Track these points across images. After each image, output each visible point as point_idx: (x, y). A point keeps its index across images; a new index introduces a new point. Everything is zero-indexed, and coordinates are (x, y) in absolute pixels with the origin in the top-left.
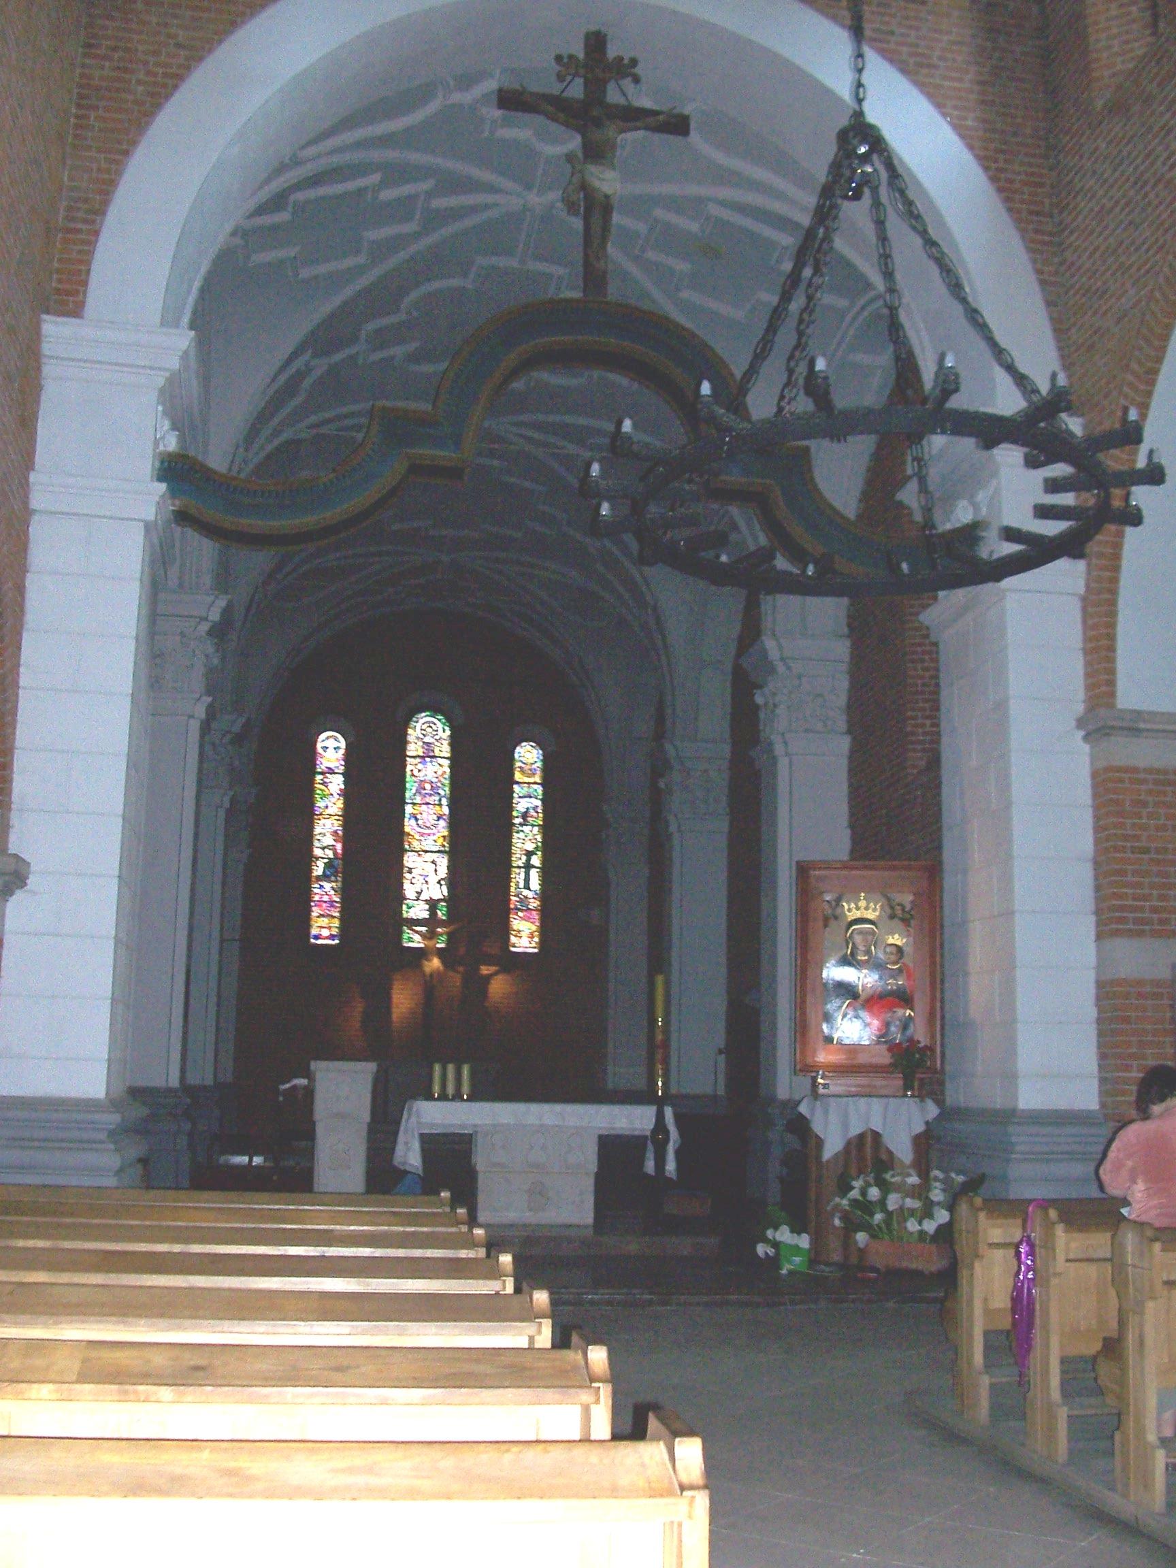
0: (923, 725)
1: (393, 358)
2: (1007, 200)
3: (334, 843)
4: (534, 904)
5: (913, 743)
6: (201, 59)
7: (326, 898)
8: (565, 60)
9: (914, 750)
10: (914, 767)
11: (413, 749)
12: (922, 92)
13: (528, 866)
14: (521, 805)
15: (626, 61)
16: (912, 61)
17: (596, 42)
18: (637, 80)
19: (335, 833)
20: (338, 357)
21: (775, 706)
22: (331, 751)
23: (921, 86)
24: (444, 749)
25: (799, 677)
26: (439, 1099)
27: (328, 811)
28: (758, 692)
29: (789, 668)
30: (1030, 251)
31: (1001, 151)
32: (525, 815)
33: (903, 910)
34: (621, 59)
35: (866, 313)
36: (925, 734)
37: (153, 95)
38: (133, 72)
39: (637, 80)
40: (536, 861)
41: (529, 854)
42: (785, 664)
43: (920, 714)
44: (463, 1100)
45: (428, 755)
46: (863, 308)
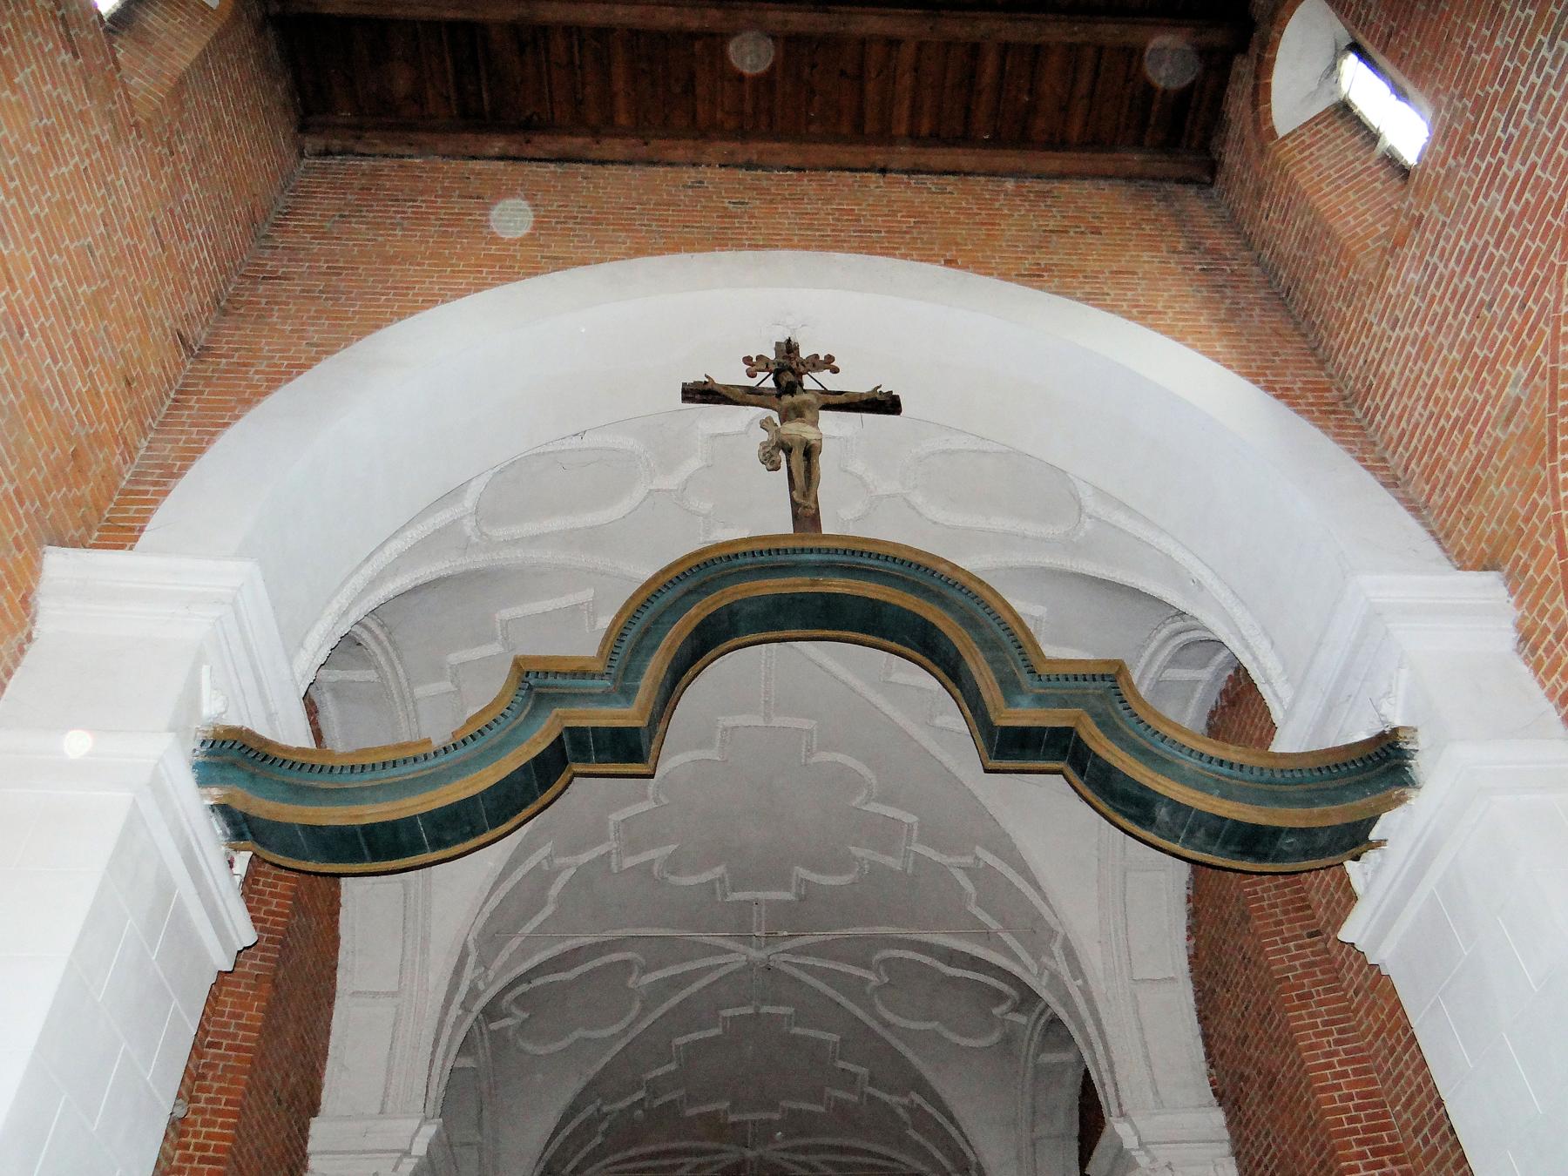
2: (1291, 404)
15: (822, 358)
17: (789, 349)
18: (835, 371)
20: (584, 858)
25: (1169, 1166)
29: (1154, 1160)
34: (817, 356)
37: (267, 380)
38: (252, 365)
39: (835, 371)
42: (1147, 1152)
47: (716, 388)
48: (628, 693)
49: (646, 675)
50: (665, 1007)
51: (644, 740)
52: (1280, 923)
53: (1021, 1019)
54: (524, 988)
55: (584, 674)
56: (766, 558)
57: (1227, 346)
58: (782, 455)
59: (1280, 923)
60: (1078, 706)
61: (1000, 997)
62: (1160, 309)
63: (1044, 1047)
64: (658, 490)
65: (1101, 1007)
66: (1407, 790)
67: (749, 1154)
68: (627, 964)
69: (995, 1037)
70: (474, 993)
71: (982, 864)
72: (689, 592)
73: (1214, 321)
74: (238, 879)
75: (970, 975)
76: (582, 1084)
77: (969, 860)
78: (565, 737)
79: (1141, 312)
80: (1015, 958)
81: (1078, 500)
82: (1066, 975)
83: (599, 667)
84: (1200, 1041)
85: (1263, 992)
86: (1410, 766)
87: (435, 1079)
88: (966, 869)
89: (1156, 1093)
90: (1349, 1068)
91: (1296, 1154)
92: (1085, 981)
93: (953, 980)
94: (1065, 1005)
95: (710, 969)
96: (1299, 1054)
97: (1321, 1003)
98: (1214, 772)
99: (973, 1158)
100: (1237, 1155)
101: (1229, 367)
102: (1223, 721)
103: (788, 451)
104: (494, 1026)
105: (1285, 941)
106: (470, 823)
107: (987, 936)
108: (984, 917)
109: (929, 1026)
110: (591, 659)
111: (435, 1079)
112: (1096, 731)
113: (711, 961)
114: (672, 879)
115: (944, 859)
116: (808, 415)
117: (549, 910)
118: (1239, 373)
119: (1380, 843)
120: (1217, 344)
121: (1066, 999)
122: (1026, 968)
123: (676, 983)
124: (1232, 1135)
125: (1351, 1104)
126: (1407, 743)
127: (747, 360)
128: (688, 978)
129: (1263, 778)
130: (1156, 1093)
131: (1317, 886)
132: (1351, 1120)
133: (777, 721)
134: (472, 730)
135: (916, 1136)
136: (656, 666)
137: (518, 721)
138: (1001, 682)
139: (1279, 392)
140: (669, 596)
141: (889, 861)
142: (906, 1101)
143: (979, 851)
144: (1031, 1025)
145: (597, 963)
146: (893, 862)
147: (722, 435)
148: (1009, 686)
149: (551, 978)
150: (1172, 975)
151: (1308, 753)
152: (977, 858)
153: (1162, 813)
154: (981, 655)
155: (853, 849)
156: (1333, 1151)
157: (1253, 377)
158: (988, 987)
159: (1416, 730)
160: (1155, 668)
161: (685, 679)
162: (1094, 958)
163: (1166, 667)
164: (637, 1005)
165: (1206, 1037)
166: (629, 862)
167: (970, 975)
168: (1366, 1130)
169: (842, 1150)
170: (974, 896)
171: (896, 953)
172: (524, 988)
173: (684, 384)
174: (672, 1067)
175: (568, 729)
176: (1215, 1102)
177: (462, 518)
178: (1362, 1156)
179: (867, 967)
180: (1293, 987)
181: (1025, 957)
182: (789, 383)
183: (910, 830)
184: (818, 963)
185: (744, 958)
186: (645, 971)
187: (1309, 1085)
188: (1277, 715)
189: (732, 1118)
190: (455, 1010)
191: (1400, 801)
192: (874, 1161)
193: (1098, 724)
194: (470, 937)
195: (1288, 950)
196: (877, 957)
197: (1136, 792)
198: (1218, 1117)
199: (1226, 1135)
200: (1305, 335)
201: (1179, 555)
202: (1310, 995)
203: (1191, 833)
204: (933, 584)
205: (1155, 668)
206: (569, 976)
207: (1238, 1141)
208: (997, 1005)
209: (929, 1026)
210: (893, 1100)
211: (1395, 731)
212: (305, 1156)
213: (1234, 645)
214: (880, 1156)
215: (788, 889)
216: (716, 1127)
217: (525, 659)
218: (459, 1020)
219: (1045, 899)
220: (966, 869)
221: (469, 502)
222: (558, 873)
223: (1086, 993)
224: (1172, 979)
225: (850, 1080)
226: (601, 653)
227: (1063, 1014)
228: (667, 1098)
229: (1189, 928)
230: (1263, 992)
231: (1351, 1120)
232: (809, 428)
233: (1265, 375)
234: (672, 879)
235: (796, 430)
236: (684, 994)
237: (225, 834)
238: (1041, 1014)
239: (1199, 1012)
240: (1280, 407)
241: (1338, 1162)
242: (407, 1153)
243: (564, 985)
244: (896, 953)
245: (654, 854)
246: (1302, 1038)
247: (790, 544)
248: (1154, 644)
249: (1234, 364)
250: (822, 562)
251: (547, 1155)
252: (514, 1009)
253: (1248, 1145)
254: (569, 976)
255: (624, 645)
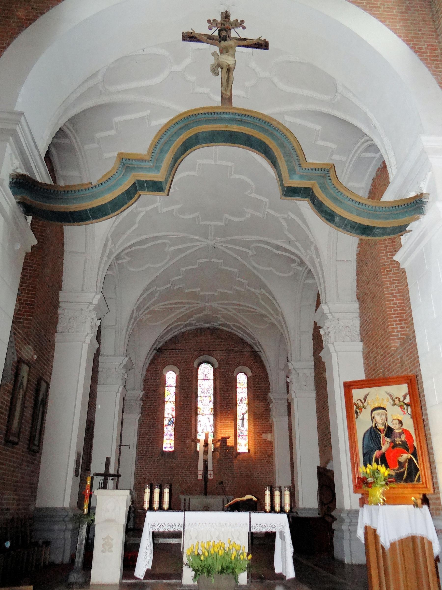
0: (397, 328)
1: (173, 210)
2: (419, 56)
3: (172, 412)
4: (246, 433)
5: (392, 336)
6: (42, 14)
7: (169, 433)
8: (212, 22)
9: (394, 339)
10: (394, 346)
11: (200, 377)
12: (375, 17)
13: (243, 419)
14: (239, 396)
15: (239, 22)
16: (368, 6)
17: (226, 16)
18: (244, 28)
19: (173, 408)
20: (149, 208)
21: (329, 332)
22: (171, 379)
23: (374, 15)
24: (211, 377)
25: (338, 319)
26: (158, 510)
27: (170, 400)
28: (321, 330)
29: (333, 317)
30: (434, 75)
31: (415, 37)
32: (241, 400)
33: (399, 400)
34: (237, 20)
35: (355, 157)
36: (398, 332)
37: (19, 26)
38: (11, 18)
39: (244, 28)
40: (246, 416)
41: (243, 414)
42: (332, 315)
43: (394, 323)
44: (266, 512)
45: (206, 379)
46: (353, 156)
47: (195, 36)
48: (158, 168)
49: (164, 161)
50: (178, 258)
51: (164, 185)
52: (386, 246)
53: (300, 269)
54: (129, 250)
55: (142, 160)
56: (209, 116)
57: (401, 26)
58: (220, 69)
59: (386, 246)
60: (314, 180)
61: (293, 261)
62: (379, 5)
63: (307, 278)
64: (174, 72)
65: (324, 268)
66: (420, 215)
67: (207, 304)
68: (165, 244)
69: (291, 273)
70: (111, 253)
71: (290, 218)
72: (181, 129)
73: (400, 13)
74: (29, 224)
75: (284, 253)
76: (150, 281)
77: (286, 216)
78: (136, 182)
79: (371, 7)
80: (299, 250)
81: (336, 87)
82: (315, 257)
83: (148, 158)
84: (356, 281)
85: (376, 268)
86: (424, 207)
87: (99, 281)
88: (284, 219)
89: (338, 297)
90: (398, 295)
91: (377, 319)
92: (320, 260)
93: (278, 255)
94: (313, 266)
95: (193, 247)
96: (383, 289)
97: (393, 274)
98: (357, 206)
99: (280, 311)
100: (360, 317)
101: (400, 36)
102: (381, 174)
103: (222, 68)
104: (119, 262)
105: (387, 252)
106: (105, 212)
107: (290, 242)
108: (290, 235)
109: (268, 269)
110: (145, 155)
111: (99, 281)
112: (319, 190)
113: (193, 244)
114: (181, 216)
115: (278, 215)
116: (230, 51)
117: (136, 226)
118: (403, 40)
119: (410, 231)
120: (397, 25)
121: (314, 266)
122: (302, 253)
123: (181, 251)
124: (360, 311)
125: (396, 305)
126: (425, 199)
127: (209, 21)
128: (187, 249)
129: (372, 210)
130: (338, 297)
131: (393, 241)
132: (395, 310)
133: (219, 162)
134: (104, 180)
135: (263, 303)
136: (168, 157)
137: (120, 177)
138: (289, 170)
139: (417, 50)
140: (174, 130)
141: (258, 214)
142: (259, 292)
143: (290, 213)
144: (304, 270)
145: (154, 243)
146: (260, 215)
147: (199, 49)
148: (292, 171)
149: (138, 247)
150: (350, 259)
151: (389, 201)
152: (289, 216)
153: (337, 219)
154: (283, 158)
155: (245, 209)
156: (387, 319)
157: (408, 41)
158: (289, 257)
159: (429, 195)
160: (359, 152)
161: (179, 161)
162: (324, 252)
163: (363, 152)
164: (168, 257)
165: (358, 281)
166: (165, 210)
167: (284, 253)
168: (399, 314)
169: (239, 305)
170: (287, 228)
171: (259, 245)
172: (129, 250)
173: (183, 33)
174: (180, 277)
175: (137, 180)
176: (357, 300)
177: (98, 83)
178: (396, 321)
179: (249, 248)
180: (386, 268)
181: (302, 249)
182: (224, 36)
183: (266, 205)
184: (232, 246)
185: (206, 243)
186: (171, 246)
187: (385, 298)
188: (391, 178)
189: (201, 293)
190: (105, 259)
191: (417, 219)
192: (248, 309)
193: (320, 187)
194: (109, 235)
195: (387, 255)
196: (252, 246)
197: (329, 212)
198: (357, 305)
199: (358, 311)
200: (434, 21)
201: (370, 115)
202: (391, 271)
203: (346, 226)
204: (271, 130)
205: (359, 152)
206: (145, 247)
207: (361, 313)
208: (293, 263)
209: (268, 269)
210: (257, 291)
211: (422, 194)
212: (58, 302)
213: (382, 151)
214: (251, 308)
215: (222, 222)
216: (195, 296)
217: (122, 154)
218: (107, 262)
219: (310, 231)
220: (284, 219)
221: (100, 77)
222: (139, 213)
223: (320, 263)
224: (350, 261)
225: (241, 284)
226: (148, 153)
227: (312, 270)
228: (179, 286)
229: (359, 244)
230: (376, 268)
231: (395, 310)
232: (230, 58)
233: (413, 41)
234: (181, 216)
235: (227, 59)
236: (184, 254)
237: (23, 210)
238: (306, 269)
239: (357, 272)
240: (415, 57)
241: (388, 322)
242: (91, 303)
243: (145, 249)
244: (259, 245)
245: (173, 207)
246: (385, 284)
247: (220, 110)
248: (359, 144)
249: (402, 35)
250: (230, 118)
251: (138, 303)
252: (125, 257)
253: (364, 315)
254: (145, 247)
255: (157, 150)
